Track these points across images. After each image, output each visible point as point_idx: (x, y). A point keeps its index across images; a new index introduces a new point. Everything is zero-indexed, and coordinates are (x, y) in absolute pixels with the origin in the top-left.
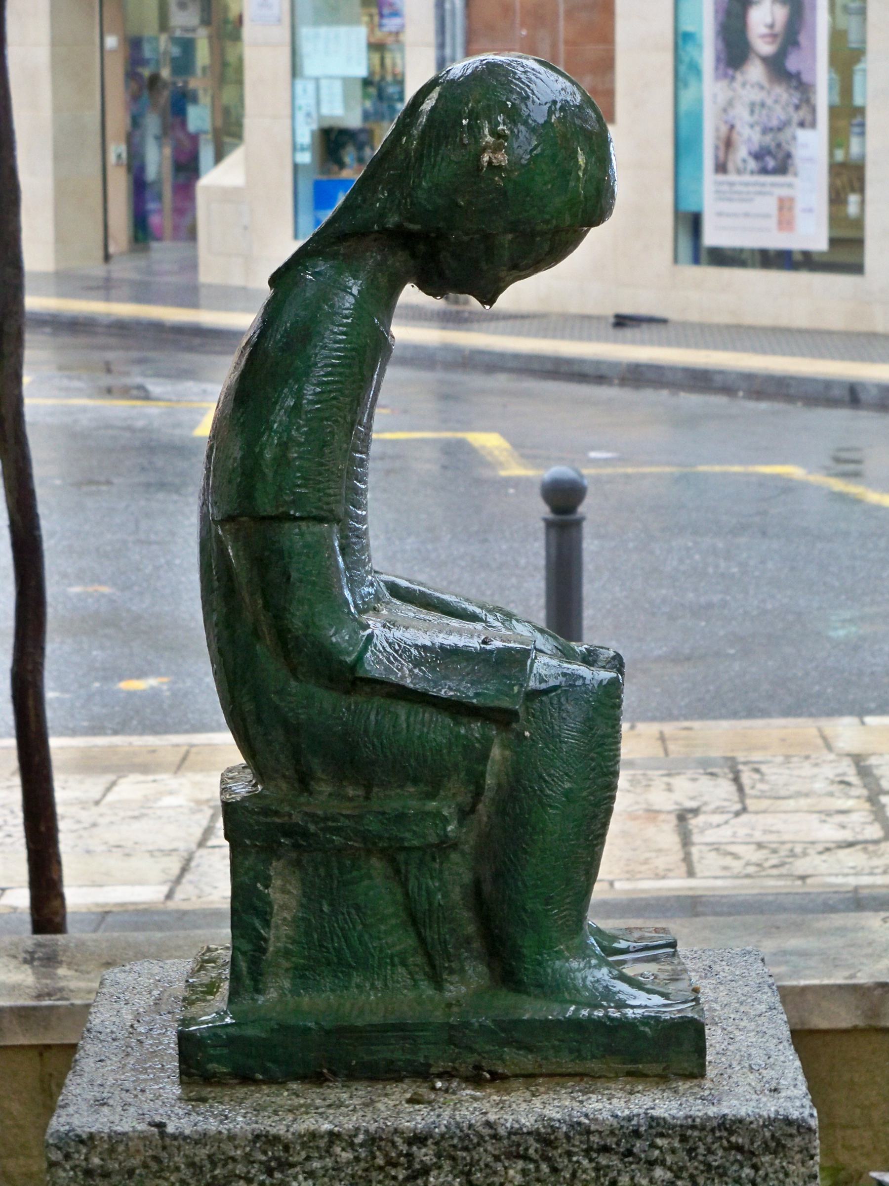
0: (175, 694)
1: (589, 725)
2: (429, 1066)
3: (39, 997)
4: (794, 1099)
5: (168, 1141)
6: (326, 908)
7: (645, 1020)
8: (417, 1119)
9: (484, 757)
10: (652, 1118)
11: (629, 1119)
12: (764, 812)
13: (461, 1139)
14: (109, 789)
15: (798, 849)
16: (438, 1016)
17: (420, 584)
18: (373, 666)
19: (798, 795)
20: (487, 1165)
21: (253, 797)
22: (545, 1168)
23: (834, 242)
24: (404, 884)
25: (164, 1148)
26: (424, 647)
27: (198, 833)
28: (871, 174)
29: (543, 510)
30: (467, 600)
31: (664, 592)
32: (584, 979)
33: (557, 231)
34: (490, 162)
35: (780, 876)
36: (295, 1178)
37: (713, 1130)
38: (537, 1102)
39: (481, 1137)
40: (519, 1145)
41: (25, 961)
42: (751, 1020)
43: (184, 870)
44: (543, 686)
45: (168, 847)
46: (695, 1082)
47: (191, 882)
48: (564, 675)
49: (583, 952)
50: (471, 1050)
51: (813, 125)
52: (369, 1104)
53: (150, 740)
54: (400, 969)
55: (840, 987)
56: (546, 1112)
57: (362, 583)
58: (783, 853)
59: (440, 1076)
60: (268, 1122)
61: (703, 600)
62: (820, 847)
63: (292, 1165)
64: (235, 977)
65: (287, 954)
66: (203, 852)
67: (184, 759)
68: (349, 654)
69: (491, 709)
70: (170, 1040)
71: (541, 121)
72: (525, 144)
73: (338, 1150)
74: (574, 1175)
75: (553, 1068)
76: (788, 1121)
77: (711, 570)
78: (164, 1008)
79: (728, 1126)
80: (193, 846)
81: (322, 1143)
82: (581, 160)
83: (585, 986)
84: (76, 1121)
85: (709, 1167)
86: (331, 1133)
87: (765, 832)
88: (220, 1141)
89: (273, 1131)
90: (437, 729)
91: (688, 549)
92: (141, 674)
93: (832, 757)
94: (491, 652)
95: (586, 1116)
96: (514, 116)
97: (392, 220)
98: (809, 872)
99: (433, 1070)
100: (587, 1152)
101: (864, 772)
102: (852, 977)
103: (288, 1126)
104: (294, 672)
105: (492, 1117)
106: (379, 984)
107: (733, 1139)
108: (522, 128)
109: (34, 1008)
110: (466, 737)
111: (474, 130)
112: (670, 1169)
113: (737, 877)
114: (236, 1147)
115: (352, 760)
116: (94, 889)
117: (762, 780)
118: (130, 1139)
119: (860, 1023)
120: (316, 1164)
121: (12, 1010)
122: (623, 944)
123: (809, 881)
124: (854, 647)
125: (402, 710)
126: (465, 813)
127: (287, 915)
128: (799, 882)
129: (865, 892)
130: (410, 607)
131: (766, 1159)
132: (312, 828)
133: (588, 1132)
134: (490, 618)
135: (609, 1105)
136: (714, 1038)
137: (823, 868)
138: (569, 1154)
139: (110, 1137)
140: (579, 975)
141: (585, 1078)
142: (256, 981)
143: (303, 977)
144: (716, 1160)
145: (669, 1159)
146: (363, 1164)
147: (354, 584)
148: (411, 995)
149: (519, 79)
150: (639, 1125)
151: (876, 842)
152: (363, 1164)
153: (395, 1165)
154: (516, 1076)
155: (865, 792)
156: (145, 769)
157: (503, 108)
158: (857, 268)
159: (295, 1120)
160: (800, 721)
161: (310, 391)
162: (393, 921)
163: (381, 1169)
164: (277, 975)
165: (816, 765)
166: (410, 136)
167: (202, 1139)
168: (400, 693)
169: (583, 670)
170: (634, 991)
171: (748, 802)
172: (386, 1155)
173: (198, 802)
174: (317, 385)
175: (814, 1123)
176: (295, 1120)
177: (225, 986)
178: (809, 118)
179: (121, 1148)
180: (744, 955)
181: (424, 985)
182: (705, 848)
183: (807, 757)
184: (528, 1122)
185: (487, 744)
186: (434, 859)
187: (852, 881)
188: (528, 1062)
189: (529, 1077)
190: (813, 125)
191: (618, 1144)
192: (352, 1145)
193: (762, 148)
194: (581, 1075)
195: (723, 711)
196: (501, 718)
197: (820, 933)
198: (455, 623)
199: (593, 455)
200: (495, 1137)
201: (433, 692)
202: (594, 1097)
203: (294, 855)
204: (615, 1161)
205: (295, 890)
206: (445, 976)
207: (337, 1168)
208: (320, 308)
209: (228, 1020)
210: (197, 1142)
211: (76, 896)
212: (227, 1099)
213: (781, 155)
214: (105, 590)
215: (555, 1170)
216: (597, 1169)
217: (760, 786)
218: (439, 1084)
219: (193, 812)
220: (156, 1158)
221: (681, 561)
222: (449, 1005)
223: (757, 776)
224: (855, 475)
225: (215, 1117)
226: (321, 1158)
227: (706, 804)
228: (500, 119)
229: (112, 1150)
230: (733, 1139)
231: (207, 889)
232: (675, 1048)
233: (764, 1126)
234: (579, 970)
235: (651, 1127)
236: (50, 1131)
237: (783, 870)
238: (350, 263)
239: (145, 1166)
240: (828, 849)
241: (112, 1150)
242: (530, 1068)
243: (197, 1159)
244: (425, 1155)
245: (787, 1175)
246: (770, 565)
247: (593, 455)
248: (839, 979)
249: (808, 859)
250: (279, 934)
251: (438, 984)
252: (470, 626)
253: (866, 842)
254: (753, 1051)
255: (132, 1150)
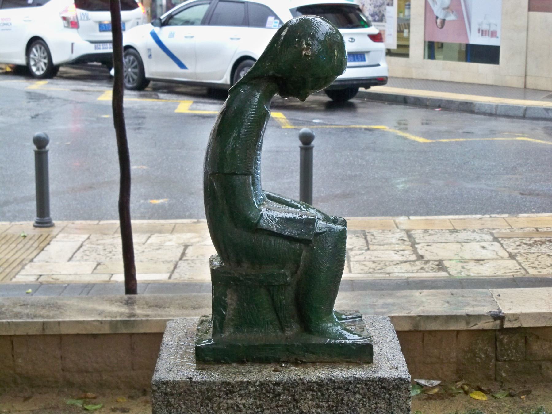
0: (169, 205)
1: (335, 245)
2: (280, 359)
3: (130, 317)
4: (402, 371)
5: (193, 384)
6: (245, 305)
7: (353, 344)
8: (276, 377)
9: (300, 255)
10: (356, 378)
11: (348, 378)
12: (375, 250)
13: (291, 384)
14: (148, 239)
15: (387, 264)
16: (283, 342)
17: (278, 195)
18: (263, 224)
19: (387, 244)
20: (300, 393)
21: (221, 267)
22: (319, 394)
23: (399, 46)
24: (272, 298)
25: (192, 386)
26: (280, 218)
27: (179, 255)
28: (412, 23)
29: (300, 143)
30: (294, 201)
31: (340, 170)
32: (333, 330)
33: (326, 78)
34: (305, 54)
35: (381, 273)
36: (236, 396)
37: (376, 382)
38: (317, 371)
39: (298, 384)
40: (311, 386)
41: (125, 304)
42: (387, 343)
43: (175, 268)
44: (321, 231)
45: (169, 260)
46: (370, 365)
47: (177, 273)
48: (328, 227)
49: (332, 321)
50: (294, 353)
51: (392, 5)
52: (260, 371)
53: (162, 222)
54: (271, 326)
55: (405, 316)
56: (320, 375)
57: (258, 196)
58: (382, 265)
59: (284, 362)
60: (226, 378)
61: (353, 174)
62: (395, 263)
63: (234, 392)
64: (214, 327)
65: (232, 320)
66: (180, 262)
67: (173, 229)
68: (255, 220)
69: (303, 240)
70: (193, 350)
71: (322, 39)
72: (316, 47)
73: (250, 387)
74: (329, 396)
75: (322, 360)
76: (401, 379)
77: (356, 163)
78: (189, 336)
79: (381, 380)
80: (178, 260)
81: (245, 385)
82: (336, 53)
83: (333, 333)
84: (162, 377)
85: (374, 394)
86: (248, 382)
87: (376, 257)
88: (210, 384)
89: (228, 381)
90: (285, 245)
91: (348, 155)
92: (158, 198)
93: (398, 230)
94: (303, 220)
95: (334, 377)
96: (313, 37)
97: (271, 73)
98: (391, 271)
99: (281, 360)
100: (334, 389)
101: (410, 236)
102: (409, 313)
103: (233, 379)
104: (236, 226)
105: (302, 377)
106: (263, 331)
107: (383, 385)
108: (316, 42)
109: (129, 321)
110: (294, 249)
111: (300, 43)
112: (361, 395)
113: (366, 273)
114: (216, 386)
115: (255, 256)
116: (143, 275)
117: (374, 238)
118: (180, 383)
119: (412, 329)
120: (243, 392)
121: (121, 321)
122: (344, 317)
123: (391, 275)
124: (406, 191)
125: (272, 239)
126: (293, 274)
127: (232, 307)
128: (387, 275)
129: (411, 279)
130: (275, 203)
131: (394, 392)
132: (241, 278)
133: (334, 382)
134: (302, 207)
135: (341, 373)
136: (376, 349)
137: (396, 270)
138: (328, 389)
139: (173, 382)
140: (331, 329)
141: (333, 363)
142: (221, 329)
143: (237, 328)
144: (377, 392)
145: (361, 392)
146: (258, 392)
147: (257, 196)
148: (274, 334)
149: (315, 25)
150: (351, 380)
151: (414, 261)
152: (258, 392)
153: (269, 393)
154: (309, 362)
155: (410, 243)
156: (160, 232)
157: (309, 35)
158: (407, 55)
159: (235, 377)
160: (387, 217)
161: (243, 131)
162: (268, 310)
163: (264, 394)
164: (228, 327)
165: (393, 233)
166: (278, 44)
167: (204, 383)
168: (271, 233)
169: (333, 226)
170: (349, 334)
171: (370, 246)
172: (266, 389)
173: (179, 244)
174: (245, 129)
175: (410, 380)
176: (235, 377)
177: (211, 330)
178: (390, 2)
179: (177, 386)
180: (384, 319)
181: (278, 331)
182: (355, 263)
183: (390, 231)
184: (314, 379)
185: (301, 250)
186: (282, 289)
187: (407, 275)
188: (313, 358)
189: (314, 363)
190: (392, 5)
191: (344, 386)
192: (255, 386)
193: (374, 13)
194: (331, 362)
195: (361, 213)
196: (307, 242)
197: (399, 297)
198: (290, 209)
199: (314, 121)
200: (303, 383)
201: (283, 233)
202: (336, 370)
203: (234, 287)
204: (343, 392)
205: (235, 298)
206: (286, 328)
207: (250, 393)
208: (246, 102)
209: (212, 342)
210: (203, 384)
211: (140, 277)
212: (212, 369)
213: (380, 15)
214: (145, 167)
215: (323, 395)
216: (337, 394)
217: (374, 241)
218: (283, 365)
219: (178, 247)
220: (189, 390)
221: (346, 160)
222: (287, 338)
223: (372, 237)
224: (405, 129)
225: (208, 375)
226: (244, 390)
227: (355, 247)
228: (309, 39)
229: (174, 386)
230: (383, 385)
231: (183, 275)
232: (363, 353)
233: (393, 381)
234: (331, 327)
235: (355, 381)
236: (153, 380)
237: (382, 271)
238: (256, 87)
239: (185, 392)
240: (397, 264)
241: (174, 386)
242: (314, 360)
243: (203, 390)
244: (279, 389)
245: (400, 397)
246: (376, 162)
247: (314, 121)
248: (404, 313)
249: (391, 267)
250: (229, 313)
251: (282, 329)
252: (295, 210)
253: (410, 261)
254: (388, 354)
255: (181, 386)
